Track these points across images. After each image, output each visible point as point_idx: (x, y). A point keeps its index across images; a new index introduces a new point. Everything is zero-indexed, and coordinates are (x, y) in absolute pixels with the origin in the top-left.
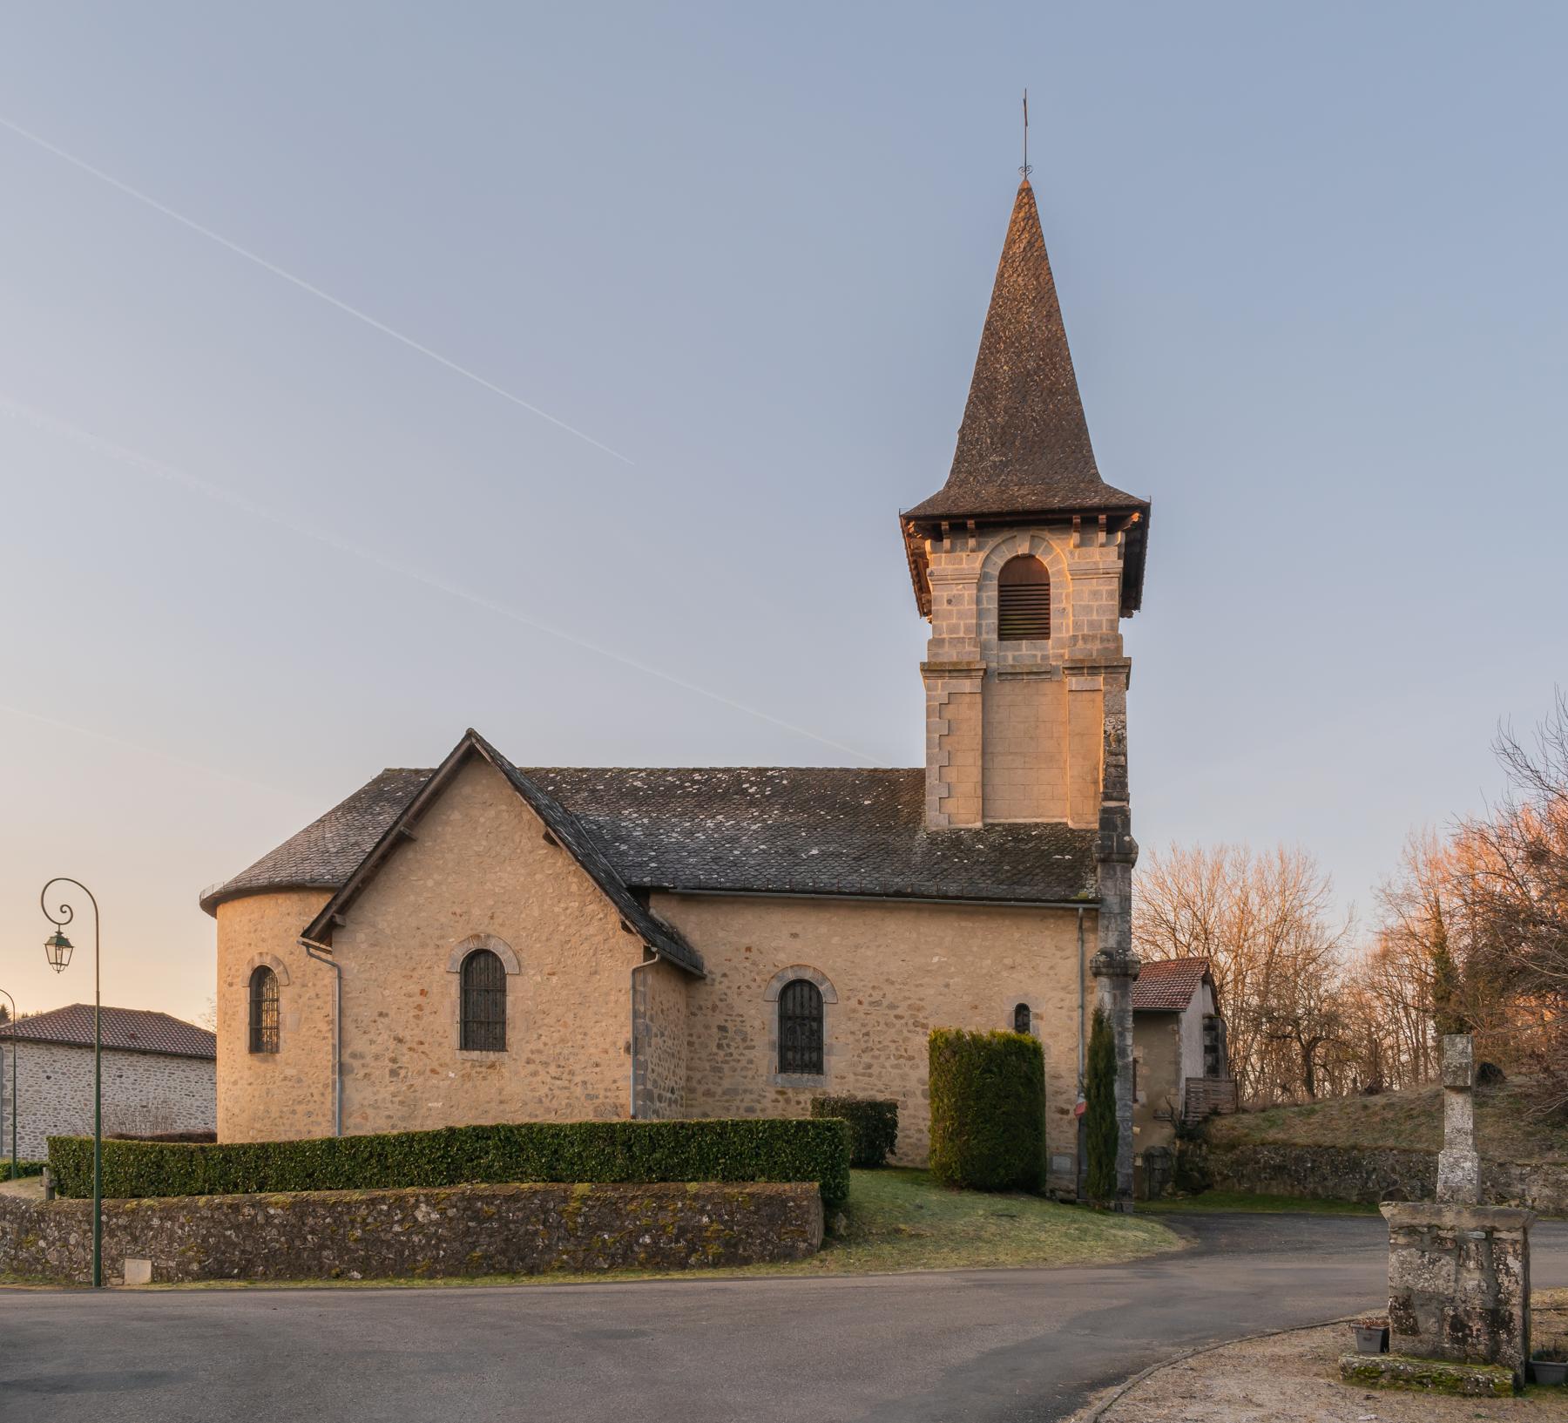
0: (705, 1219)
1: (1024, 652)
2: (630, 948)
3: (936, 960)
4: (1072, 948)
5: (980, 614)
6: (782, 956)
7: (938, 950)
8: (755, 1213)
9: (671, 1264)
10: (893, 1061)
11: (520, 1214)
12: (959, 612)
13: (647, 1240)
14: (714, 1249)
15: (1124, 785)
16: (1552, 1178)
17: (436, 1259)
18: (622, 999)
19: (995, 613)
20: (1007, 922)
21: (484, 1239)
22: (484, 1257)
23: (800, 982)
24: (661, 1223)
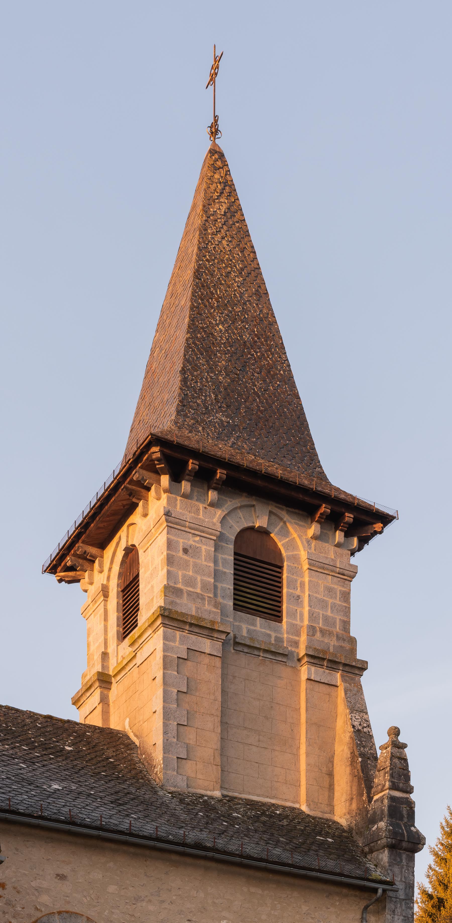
1: (258, 628)
5: (217, 575)
6: (45, 899)
12: (195, 565)
15: (407, 778)
19: (231, 578)
20: (295, 894)
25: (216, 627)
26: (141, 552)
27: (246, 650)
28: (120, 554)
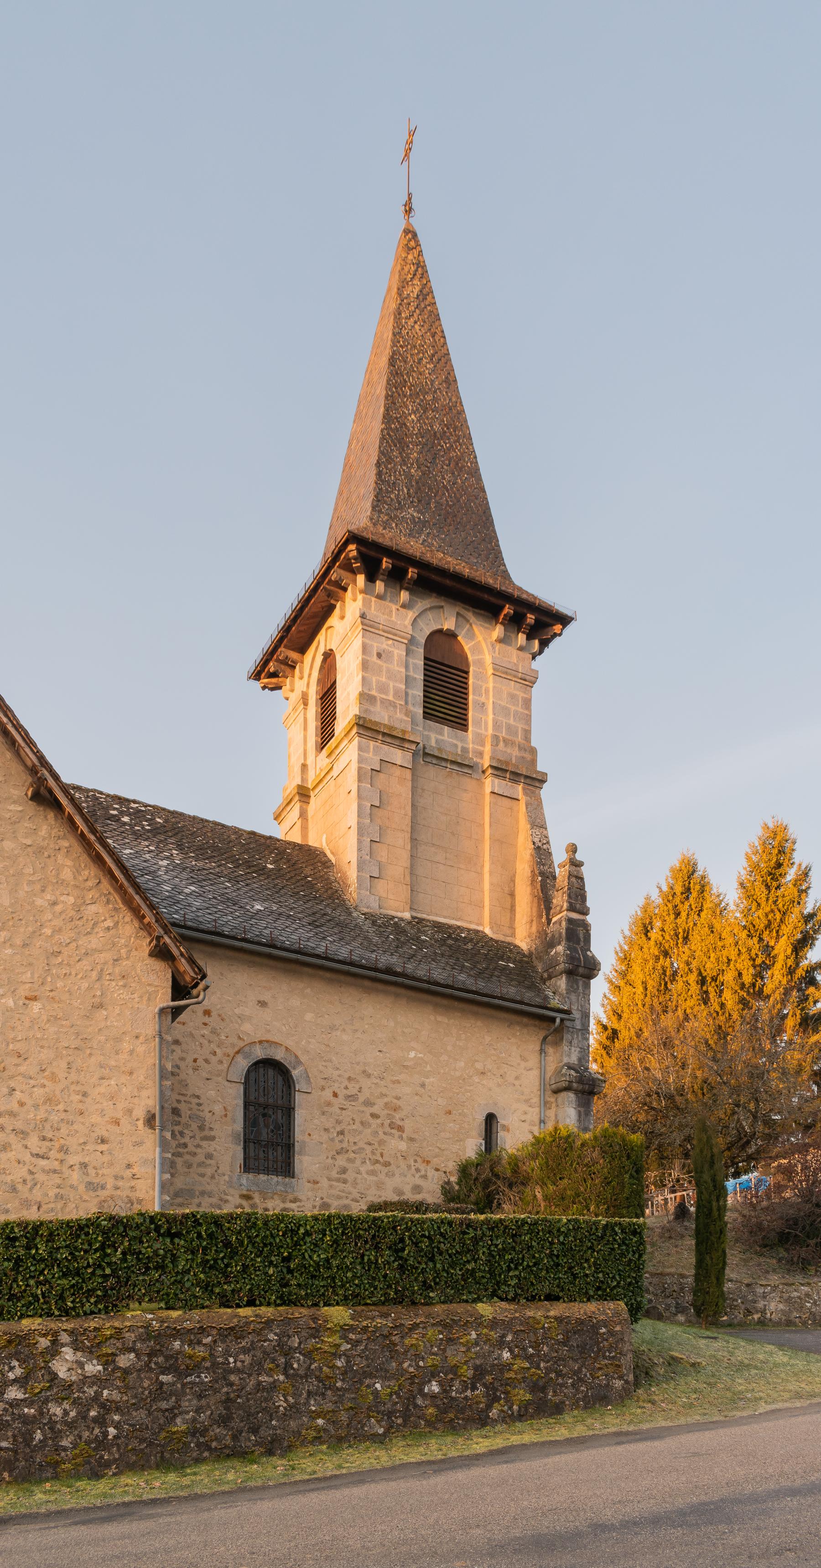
0: (506, 1355)
1: (446, 738)
2: (153, 978)
3: (412, 1054)
4: (533, 1060)
5: (408, 680)
6: (247, 1027)
7: (413, 1044)
8: (564, 1344)
9: (467, 1420)
10: (369, 1166)
11: (247, 1359)
13: (435, 1388)
14: (522, 1395)
15: (584, 899)
16: (786, 1296)
17: (102, 1443)
18: (141, 1049)
19: (421, 684)
20: (479, 1023)
21: (188, 1403)
22: (194, 1431)
23: (269, 1063)
24: (453, 1361)
25: (407, 737)
26: (338, 657)
27: (434, 762)
28: (319, 659)
